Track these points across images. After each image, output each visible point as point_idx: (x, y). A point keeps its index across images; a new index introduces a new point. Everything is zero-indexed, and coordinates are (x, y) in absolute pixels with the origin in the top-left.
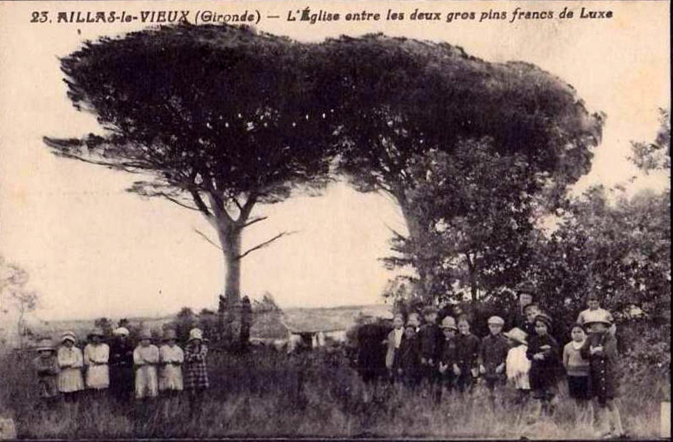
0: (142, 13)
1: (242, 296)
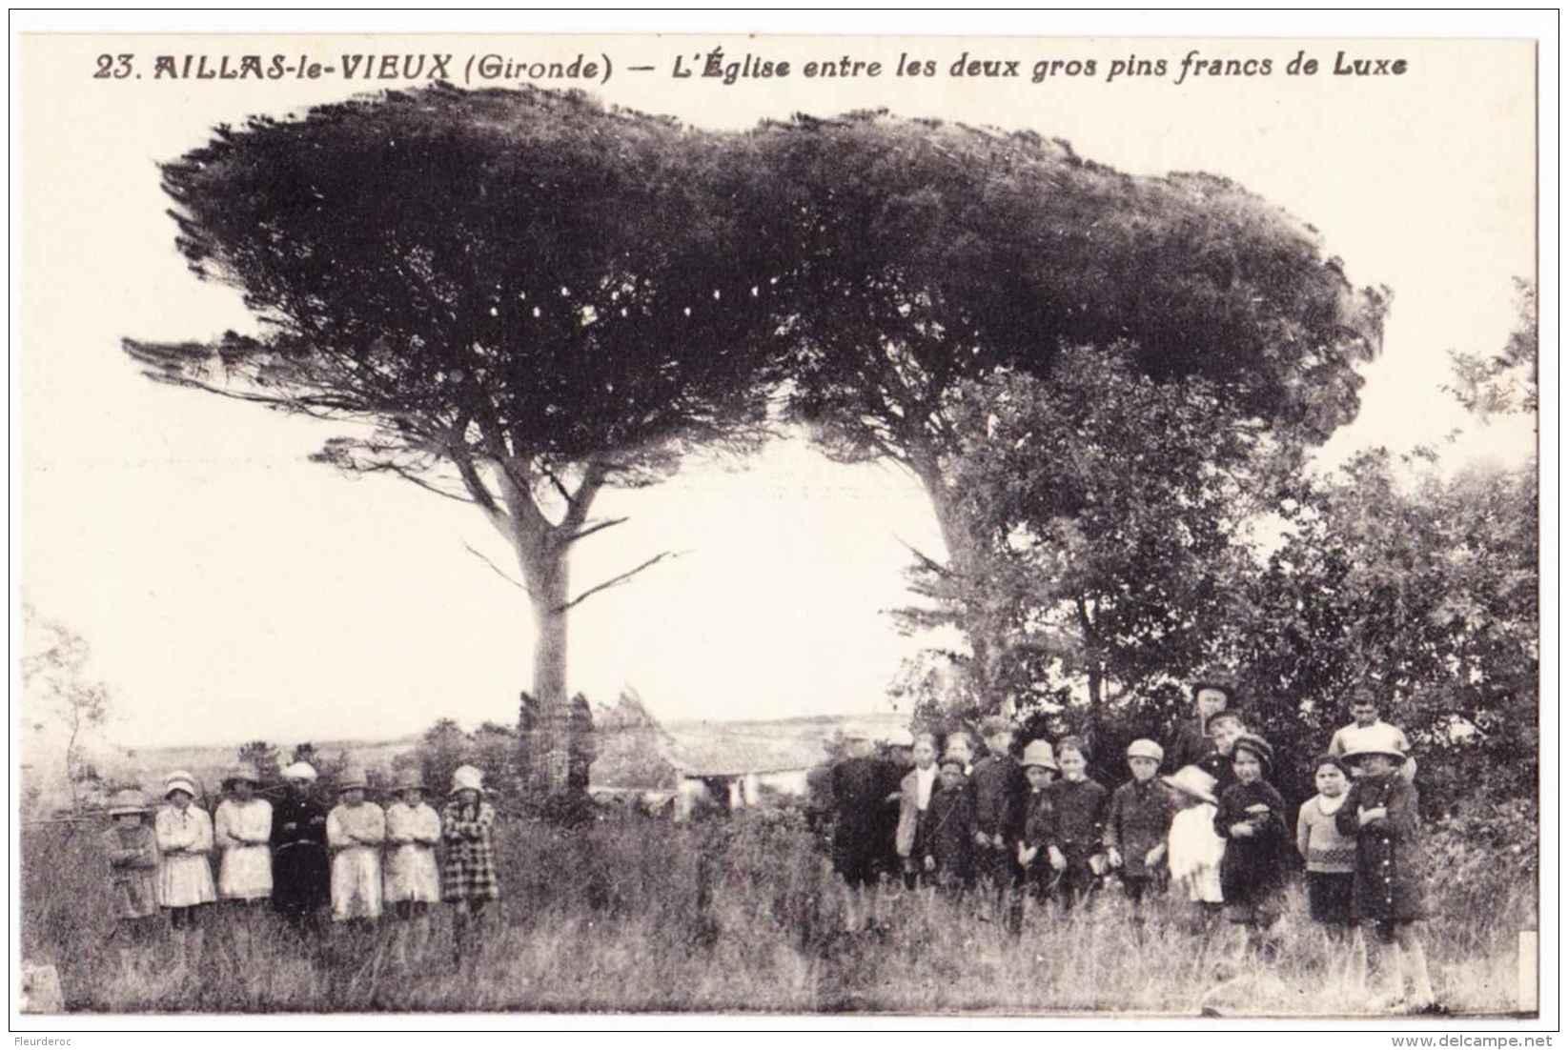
0: (345, 58)
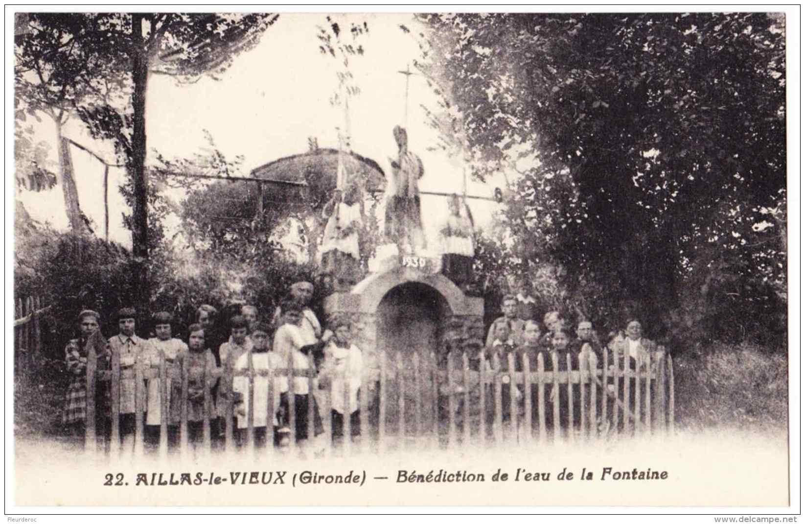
0: (232, 474)
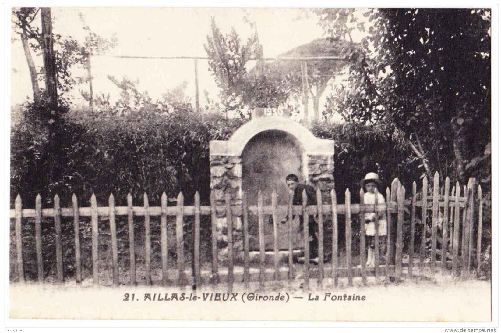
0: (204, 294)
1: (244, 67)
